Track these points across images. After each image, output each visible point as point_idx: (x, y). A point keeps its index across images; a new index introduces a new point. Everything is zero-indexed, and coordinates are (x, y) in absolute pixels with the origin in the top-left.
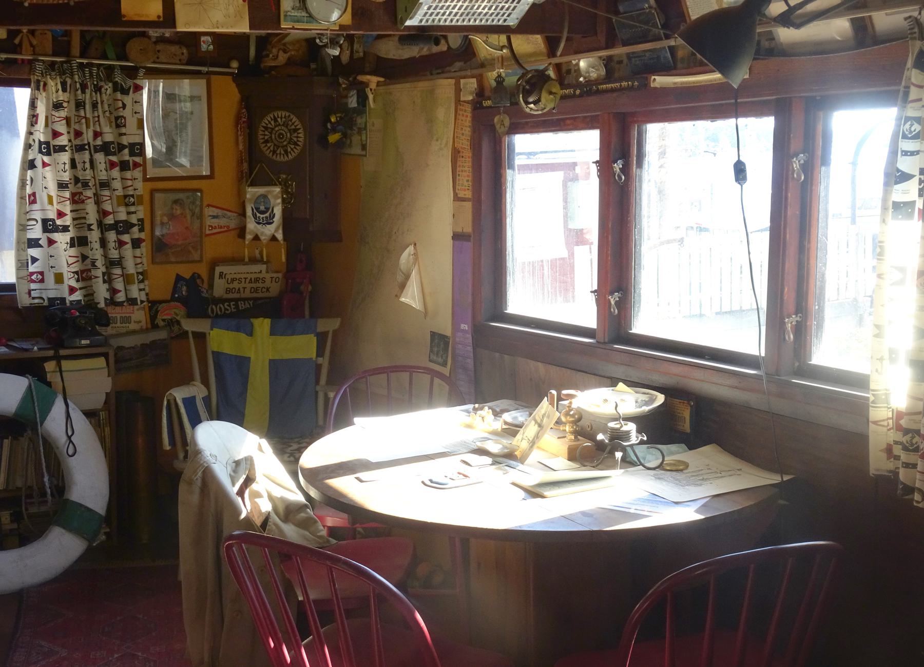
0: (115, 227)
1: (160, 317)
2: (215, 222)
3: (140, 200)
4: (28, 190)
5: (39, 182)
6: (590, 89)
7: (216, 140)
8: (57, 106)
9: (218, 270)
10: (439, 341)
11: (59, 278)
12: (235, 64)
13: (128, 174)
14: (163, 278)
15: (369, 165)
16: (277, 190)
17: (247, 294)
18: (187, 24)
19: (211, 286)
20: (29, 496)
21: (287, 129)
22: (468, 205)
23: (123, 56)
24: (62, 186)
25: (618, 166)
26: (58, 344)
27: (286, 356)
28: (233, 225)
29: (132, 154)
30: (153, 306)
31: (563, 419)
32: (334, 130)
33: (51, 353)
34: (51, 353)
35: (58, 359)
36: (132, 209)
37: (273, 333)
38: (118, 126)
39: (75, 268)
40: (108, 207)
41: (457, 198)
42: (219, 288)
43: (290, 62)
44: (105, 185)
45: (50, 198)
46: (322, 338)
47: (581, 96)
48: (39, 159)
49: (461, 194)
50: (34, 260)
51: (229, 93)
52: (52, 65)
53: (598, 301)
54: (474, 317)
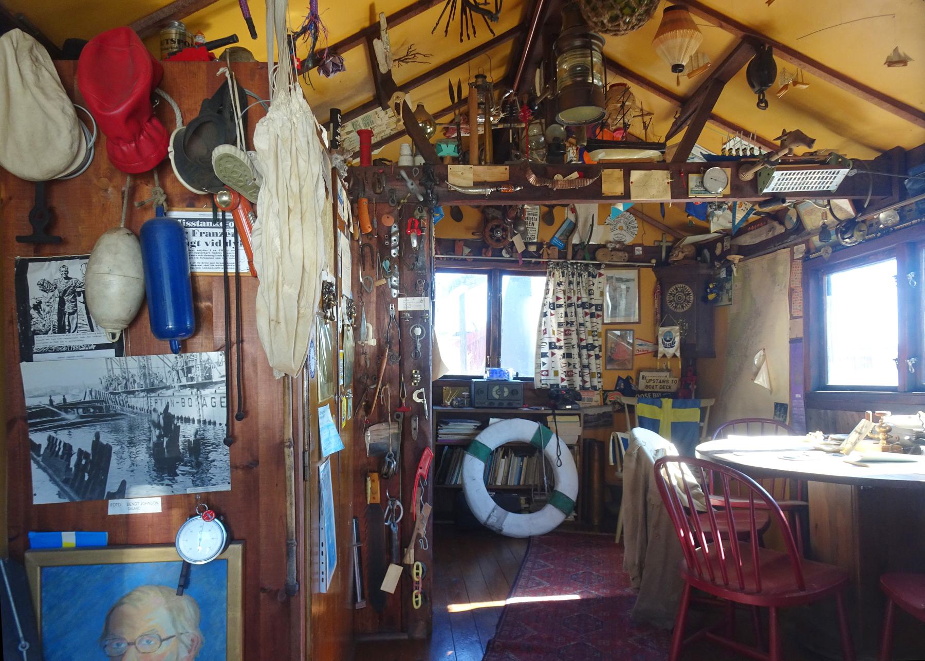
0: (586, 347)
1: (608, 399)
2: (641, 348)
3: (599, 335)
4: (543, 328)
5: (548, 323)
6: (888, 231)
7: (642, 314)
8: (559, 284)
9: (642, 374)
10: (780, 408)
11: (556, 373)
12: (654, 261)
13: (594, 320)
14: (610, 380)
15: (733, 309)
16: (677, 328)
17: (658, 389)
18: (636, 197)
19: (637, 383)
20: (536, 490)
21: (683, 295)
22: (801, 321)
23: (594, 259)
24: (560, 325)
25: (911, 276)
26: (555, 407)
27: (681, 420)
28: (650, 349)
29: (597, 310)
30: (605, 393)
31: (877, 430)
32: (711, 292)
33: (551, 412)
34: (551, 412)
35: (554, 415)
36: (596, 338)
37: (674, 407)
38: (590, 294)
39: (565, 369)
40: (583, 336)
41: (792, 318)
42: (642, 385)
43: (685, 258)
44: (582, 325)
45: (554, 332)
46: (703, 410)
47: (881, 236)
48: (549, 311)
49: (795, 315)
50: (544, 364)
51: (650, 277)
52: (558, 264)
53: (898, 367)
54: (805, 388)
